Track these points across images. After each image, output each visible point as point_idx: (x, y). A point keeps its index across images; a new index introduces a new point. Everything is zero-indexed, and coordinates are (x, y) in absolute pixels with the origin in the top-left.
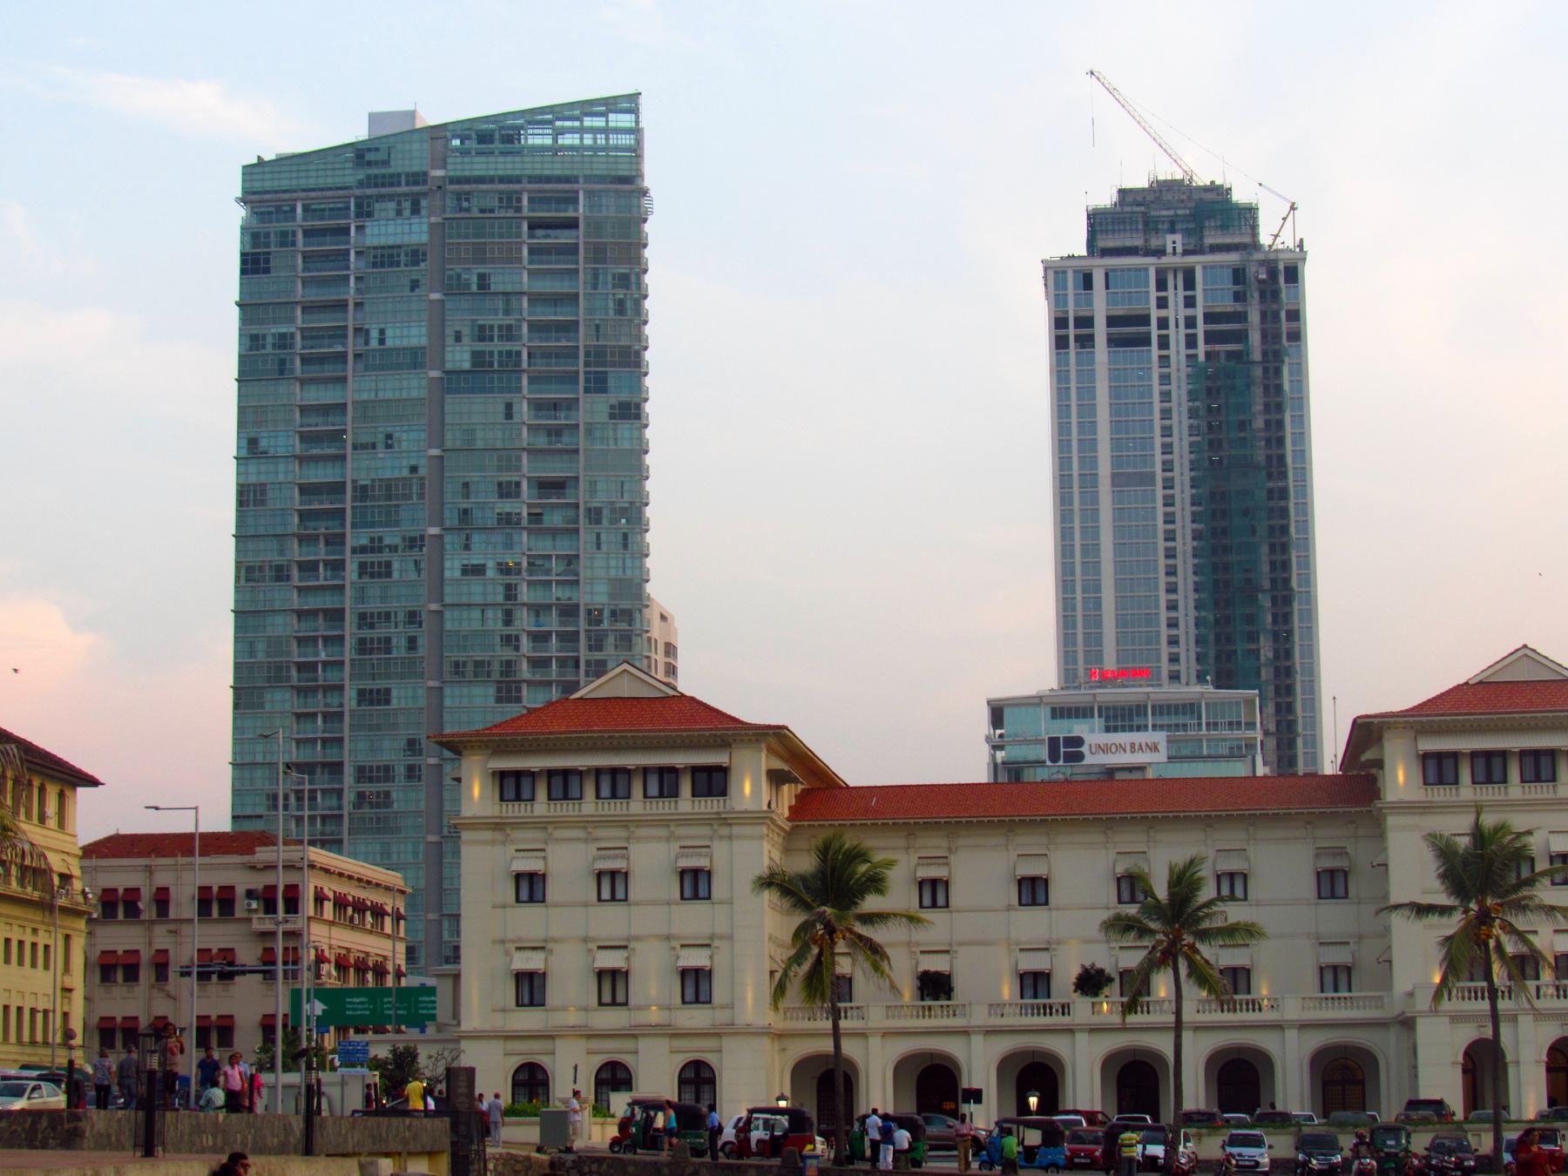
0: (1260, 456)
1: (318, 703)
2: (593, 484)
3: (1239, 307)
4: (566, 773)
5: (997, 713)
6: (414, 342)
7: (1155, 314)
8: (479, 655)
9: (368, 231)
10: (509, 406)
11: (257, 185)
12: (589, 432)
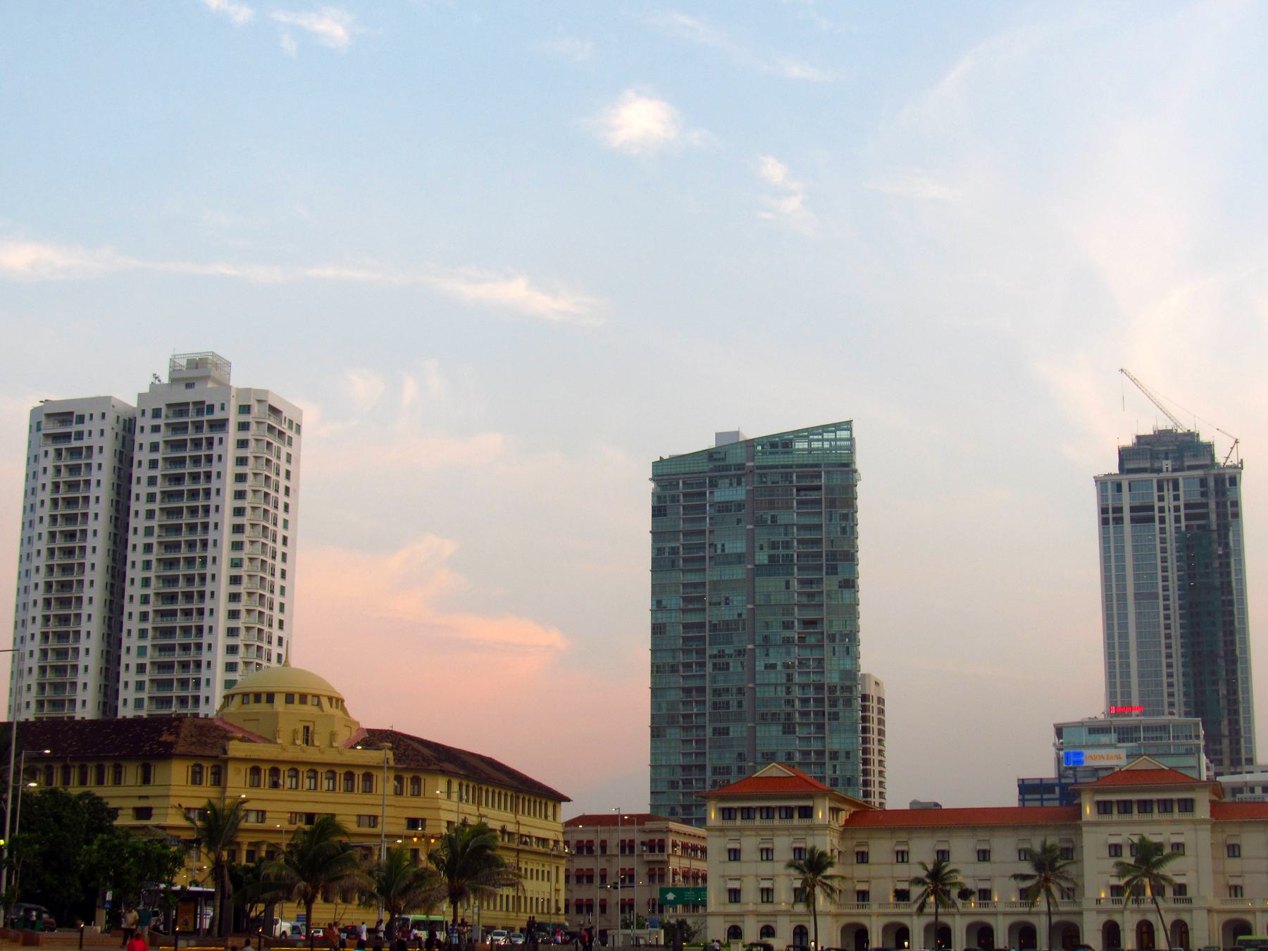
0: (1217, 583)
1: (693, 734)
2: (831, 622)
3: (1204, 500)
4: (749, 809)
5: (1059, 731)
6: (739, 550)
7: (1157, 505)
8: (774, 710)
10: (787, 583)
11: (660, 472)
12: (828, 595)
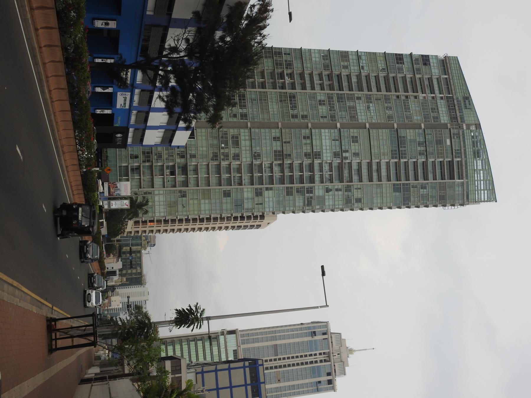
9: (442, 101)
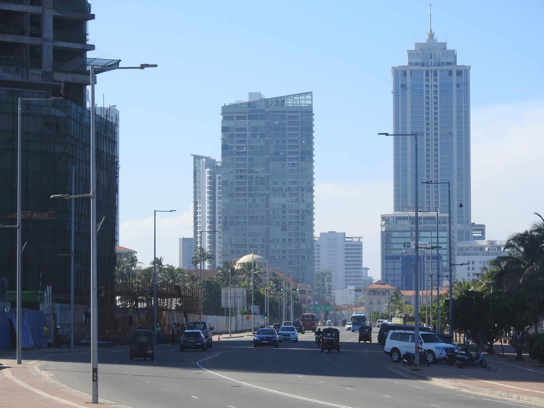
10: (284, 164)
